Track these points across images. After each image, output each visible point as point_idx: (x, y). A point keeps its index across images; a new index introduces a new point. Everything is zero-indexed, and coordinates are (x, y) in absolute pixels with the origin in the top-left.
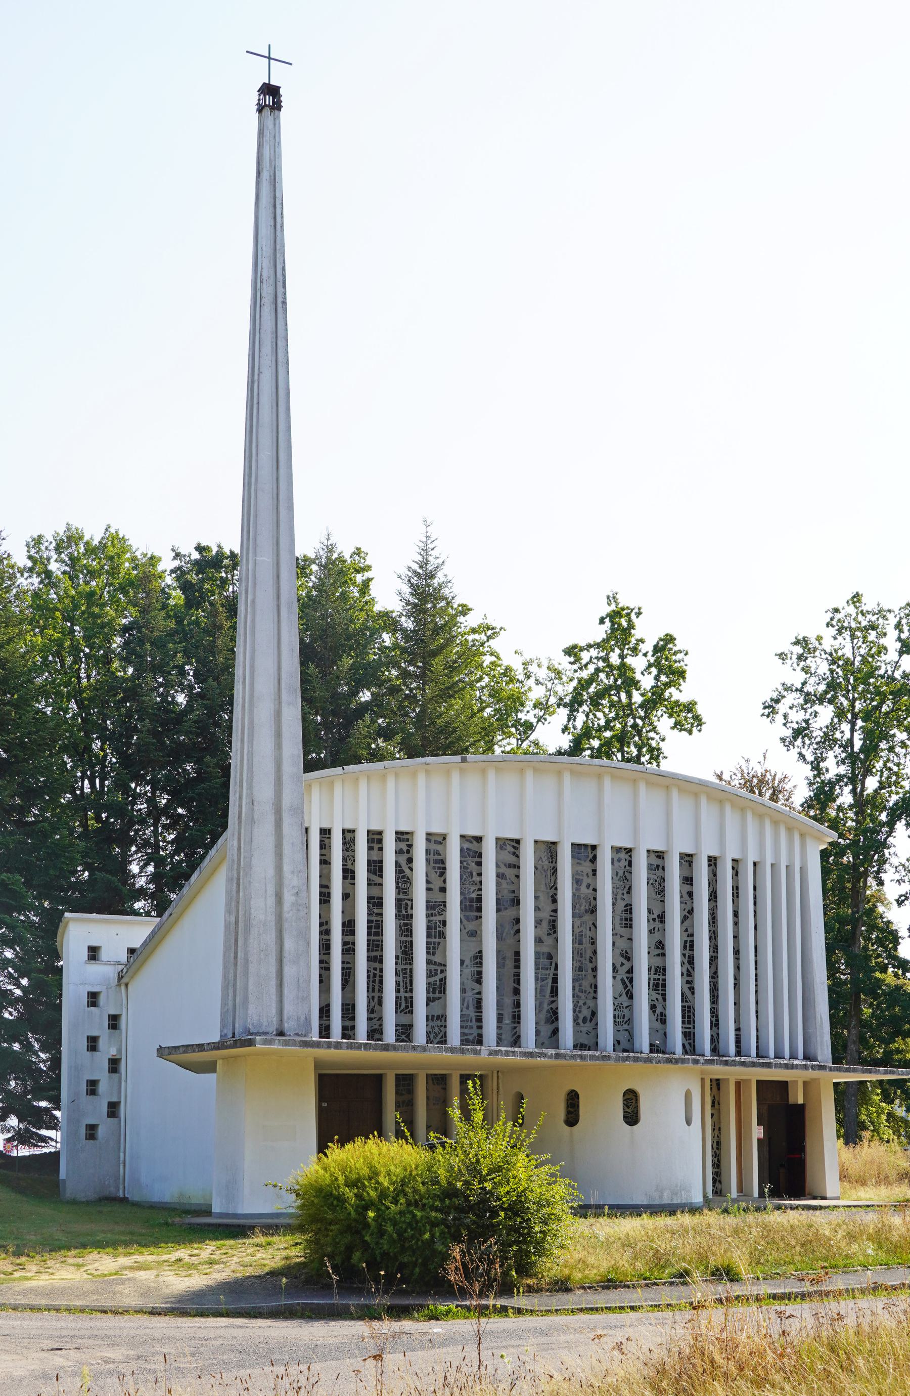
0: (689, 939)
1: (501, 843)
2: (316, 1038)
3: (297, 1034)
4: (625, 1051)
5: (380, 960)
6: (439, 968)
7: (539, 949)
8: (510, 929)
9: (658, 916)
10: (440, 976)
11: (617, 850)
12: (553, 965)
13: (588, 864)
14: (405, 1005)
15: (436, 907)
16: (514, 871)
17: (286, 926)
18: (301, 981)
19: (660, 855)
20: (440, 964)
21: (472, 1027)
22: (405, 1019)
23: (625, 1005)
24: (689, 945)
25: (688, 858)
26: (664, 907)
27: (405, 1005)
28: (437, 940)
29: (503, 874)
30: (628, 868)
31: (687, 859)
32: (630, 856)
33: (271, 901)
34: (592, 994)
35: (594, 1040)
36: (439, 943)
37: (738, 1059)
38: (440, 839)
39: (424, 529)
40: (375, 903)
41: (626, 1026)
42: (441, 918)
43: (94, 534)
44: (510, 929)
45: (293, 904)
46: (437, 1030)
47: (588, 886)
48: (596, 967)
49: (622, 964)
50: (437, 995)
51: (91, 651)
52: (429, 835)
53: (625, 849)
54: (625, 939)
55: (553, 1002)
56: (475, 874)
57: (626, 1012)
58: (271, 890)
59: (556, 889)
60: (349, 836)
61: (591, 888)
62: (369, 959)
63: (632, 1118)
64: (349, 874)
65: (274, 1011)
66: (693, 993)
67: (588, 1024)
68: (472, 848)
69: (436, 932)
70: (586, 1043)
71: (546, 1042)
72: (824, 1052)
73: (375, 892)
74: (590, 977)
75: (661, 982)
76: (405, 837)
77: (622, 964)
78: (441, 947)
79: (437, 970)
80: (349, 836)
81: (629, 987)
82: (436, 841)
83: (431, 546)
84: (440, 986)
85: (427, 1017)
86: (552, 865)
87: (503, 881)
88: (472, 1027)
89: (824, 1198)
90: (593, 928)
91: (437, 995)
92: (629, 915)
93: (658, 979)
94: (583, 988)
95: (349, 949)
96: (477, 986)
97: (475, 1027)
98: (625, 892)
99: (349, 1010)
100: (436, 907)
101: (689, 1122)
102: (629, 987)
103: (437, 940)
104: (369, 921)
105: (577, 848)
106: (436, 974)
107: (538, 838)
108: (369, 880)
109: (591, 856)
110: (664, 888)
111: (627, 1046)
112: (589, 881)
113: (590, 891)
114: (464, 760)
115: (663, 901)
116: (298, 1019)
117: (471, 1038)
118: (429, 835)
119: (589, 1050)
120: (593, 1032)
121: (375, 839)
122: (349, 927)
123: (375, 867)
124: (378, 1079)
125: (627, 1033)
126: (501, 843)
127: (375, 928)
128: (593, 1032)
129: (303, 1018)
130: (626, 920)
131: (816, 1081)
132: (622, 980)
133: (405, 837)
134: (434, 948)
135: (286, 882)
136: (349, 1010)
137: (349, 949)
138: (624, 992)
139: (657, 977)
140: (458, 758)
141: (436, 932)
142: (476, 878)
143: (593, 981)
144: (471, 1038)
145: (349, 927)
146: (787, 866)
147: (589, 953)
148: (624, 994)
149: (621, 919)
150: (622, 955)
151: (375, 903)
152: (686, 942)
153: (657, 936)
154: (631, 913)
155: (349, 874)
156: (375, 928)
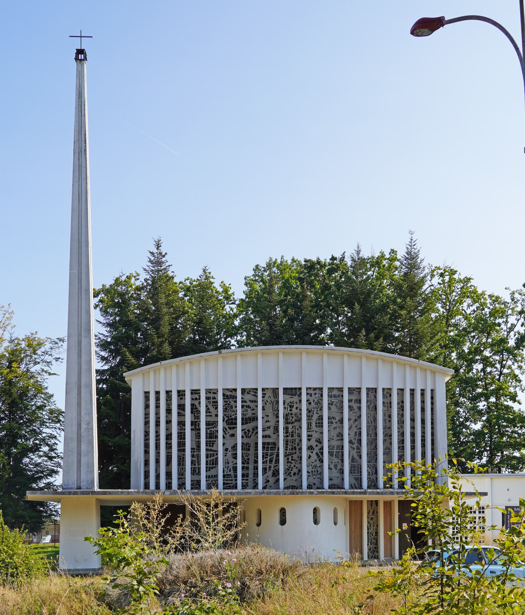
2: (96, 488)
3: (87, 488)
4: (318, 488)
5: (184, 450)
6: (215, 453)
9: (339, 421)
10: (214, 457)
12: (277, 448)
13: (297, 397)
14: (196, 471)
16: (255, 404)
17: (82, 439)
18: (89, 464)
19: (402, 390)
20: (215, 451)
21: (232, 480)
22: (196, 478)
23: (318, 465)
24: (402, 434)
25: (358, 390)
26: (343, 416)
27: (196, 471)
28: (214, 440)
29: (249, 406)
30: (320, 397)
32: (322, 392)
33: (75, 428)
34: (299, 461)
35: (300, 484)
36: (215, 441)
39: (410, 236)
41: (319, 476)
45: (86, 429)
46: (214, 482)
47: (297, 408)
48: (301, 448)
49: (317, 446)
50: (214, 466)
53: (319, 388)
54: (318, 433)
55: (276, 466)
56: (234, 407)
57: (319, 469)
58: (75, 423)
59: (278, 411)
61: (298, 409)
62: (179, 450)
63: (283, 522)
64: (169, 411)
65: (75, 478)
67: (296, 476)
70: (295, 485)
71: (272, 486)
73: (182, 419)
74: (298, 453)
76: (198, 392)
77: (317, 446)
79: (212, 454)
81: (321, 456)
83: (414, 244)
84: (216, 461)
85: (206, 476)
86: (276, 399)
88: (232, 480)
90: (299, 428)
91: (214, 466)
92: (321, 421)
93: (339, 452)
94: (294, 458)
95: (169, 446)
97: (234, 480)
98: (318, 409)
99: (169, 475)
102: (321, 456)
103: (214, 440)
106: (213, 456)
107: (264, 387)
108: (178, 413)
109: (298, 393)
110: (343, 406)
111: (319, 486)
112: (297, 406)
114: (220, 353)
115: (342, 413)
116: (88, 481)
117: (232, 485)
119: (297, 489)
120: (299, 480)
122: (169, 437)
123: (181, 407)
125: (319, 479)
126: (208, 391)
127: (181, 436)
128: (299, 480)
129: (90, 480)
130: (319, 423)
132: (317, 454)
133: (198, 392)
134: (213, 444)
135: (82, 419)
136: (169, 475)
137: (169, 446)
138: (318, 459)
139: (338, 451)
140: (217, 352)
142: (234, 409)
143: (299, 455)
144: (232, 485)
145: (169, 437)
147: (297, 441)
148: (318, 460)
149: (316, 423)
150: (317, 441)
153: (401, 431)
154: (322, 420)
155: (169, 411)
156: (181, 436)
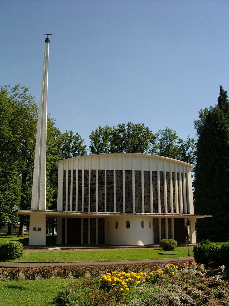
7: (92, 183)
8: (110, 189)
15: (93, 185)
31: (173, 173)
40: (80, 184)
42: (95, 187)
44: (110, 189)
49: (139, 195)
57: (140, 205)
60: (74, 171)
64: (74, 178)
69: (93, 190)
72: (192, 211)
75: (149, 198)
77: (139, 195)
80: (74, 171)
82: (70, 171)
87: (146, 185)
89: (192, 243)
96: (103, 200)
100: (93, 185)
104: (81, 190)
105: (153, 172)
106: (94, 198)
121: (80, 171)
122: (74, 189)
126: (153, 172)
131: (174, 213)
141: (93, 190)
145: (74, 189)
146: (186, 173)
147: (131, 192)
151: (80, 184)
156: (80, 189)
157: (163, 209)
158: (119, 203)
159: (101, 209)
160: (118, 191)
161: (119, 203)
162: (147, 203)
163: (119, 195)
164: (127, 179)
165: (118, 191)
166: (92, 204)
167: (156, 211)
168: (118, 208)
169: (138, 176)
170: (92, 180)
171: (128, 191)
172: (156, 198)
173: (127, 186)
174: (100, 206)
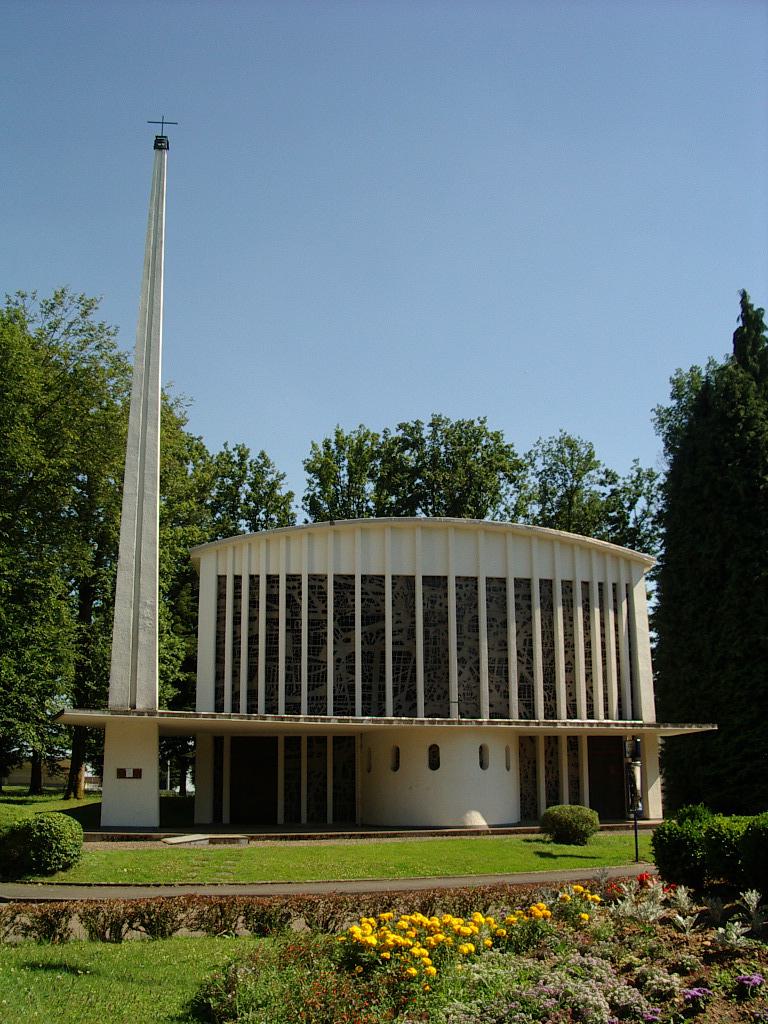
0: (528, 638)
1: (518, 582)
8: (373, 637)
11: (541, 581)
37: (605, 721)
38: (323, 578)
40: (272, 622)
43: (506, 441)
44: (373, 637)
51: (397, 495)
52: (288, 576)
60: (254, 579)
64: (254, 603)
66: (532, 676)
68: (254, 580)
69: (318, 641)
78: (323, 650)
80: (254, 579)
82: (238, 579)
100: (317, 625)
101: (508, 769)
107: (396, 574)
113: (443, 608)
118: (458, 578)
121: (272, 580)
122: (253, 639)
124: (324, 739)
125: (474, 706)
137: (253, 653)
141: (318, 641)
145: (253, 639)
151: (272, 622)
152: (525, 640)
155: (254, 603)
156: (272, 639)
157: (553, 706)
158: (403, 687)
159: (342, 707)
160: (402, 644)
161: (403, 687)
162: (499, 686)
163: (404, 659)
164: (430, 605)
165: (402, 644)
166: (313, 689)
167: (528, 711)
168: (400, 703)
169: (468, 594)
170: (312, 609)
171: (435, 643)
172: (527, 668)
173: (432, 630)
174: (340, 697)
